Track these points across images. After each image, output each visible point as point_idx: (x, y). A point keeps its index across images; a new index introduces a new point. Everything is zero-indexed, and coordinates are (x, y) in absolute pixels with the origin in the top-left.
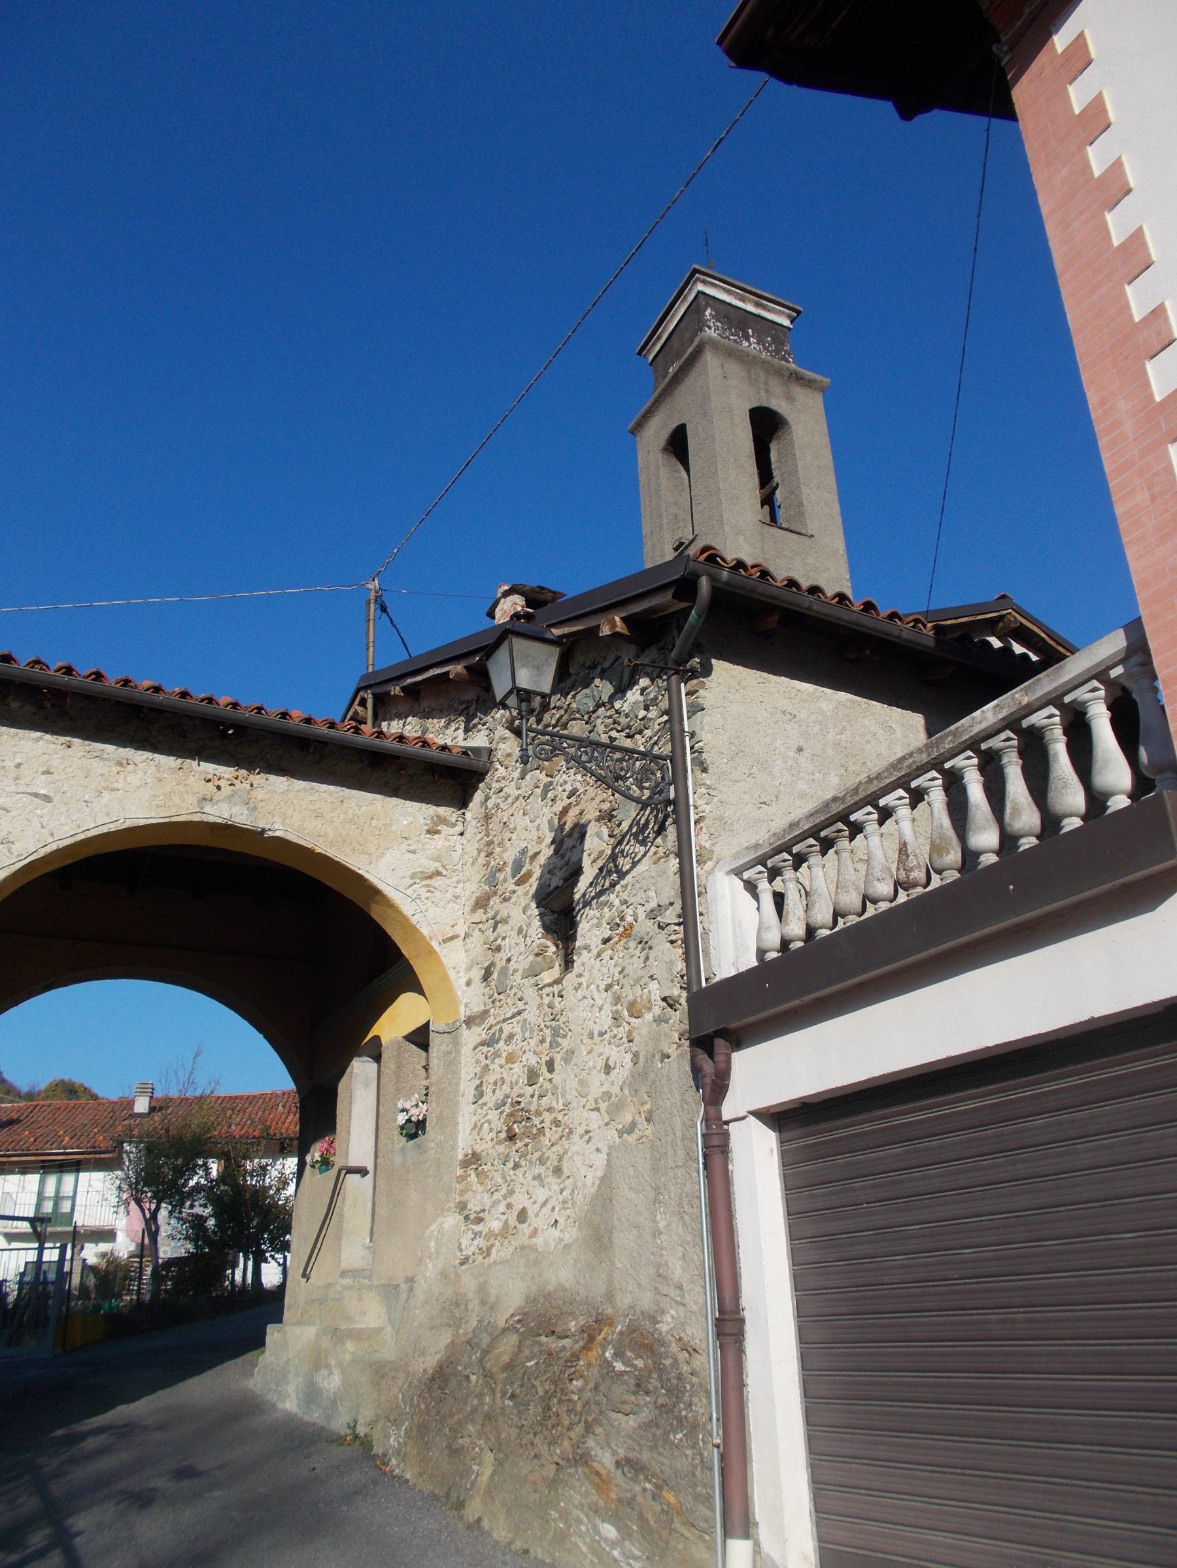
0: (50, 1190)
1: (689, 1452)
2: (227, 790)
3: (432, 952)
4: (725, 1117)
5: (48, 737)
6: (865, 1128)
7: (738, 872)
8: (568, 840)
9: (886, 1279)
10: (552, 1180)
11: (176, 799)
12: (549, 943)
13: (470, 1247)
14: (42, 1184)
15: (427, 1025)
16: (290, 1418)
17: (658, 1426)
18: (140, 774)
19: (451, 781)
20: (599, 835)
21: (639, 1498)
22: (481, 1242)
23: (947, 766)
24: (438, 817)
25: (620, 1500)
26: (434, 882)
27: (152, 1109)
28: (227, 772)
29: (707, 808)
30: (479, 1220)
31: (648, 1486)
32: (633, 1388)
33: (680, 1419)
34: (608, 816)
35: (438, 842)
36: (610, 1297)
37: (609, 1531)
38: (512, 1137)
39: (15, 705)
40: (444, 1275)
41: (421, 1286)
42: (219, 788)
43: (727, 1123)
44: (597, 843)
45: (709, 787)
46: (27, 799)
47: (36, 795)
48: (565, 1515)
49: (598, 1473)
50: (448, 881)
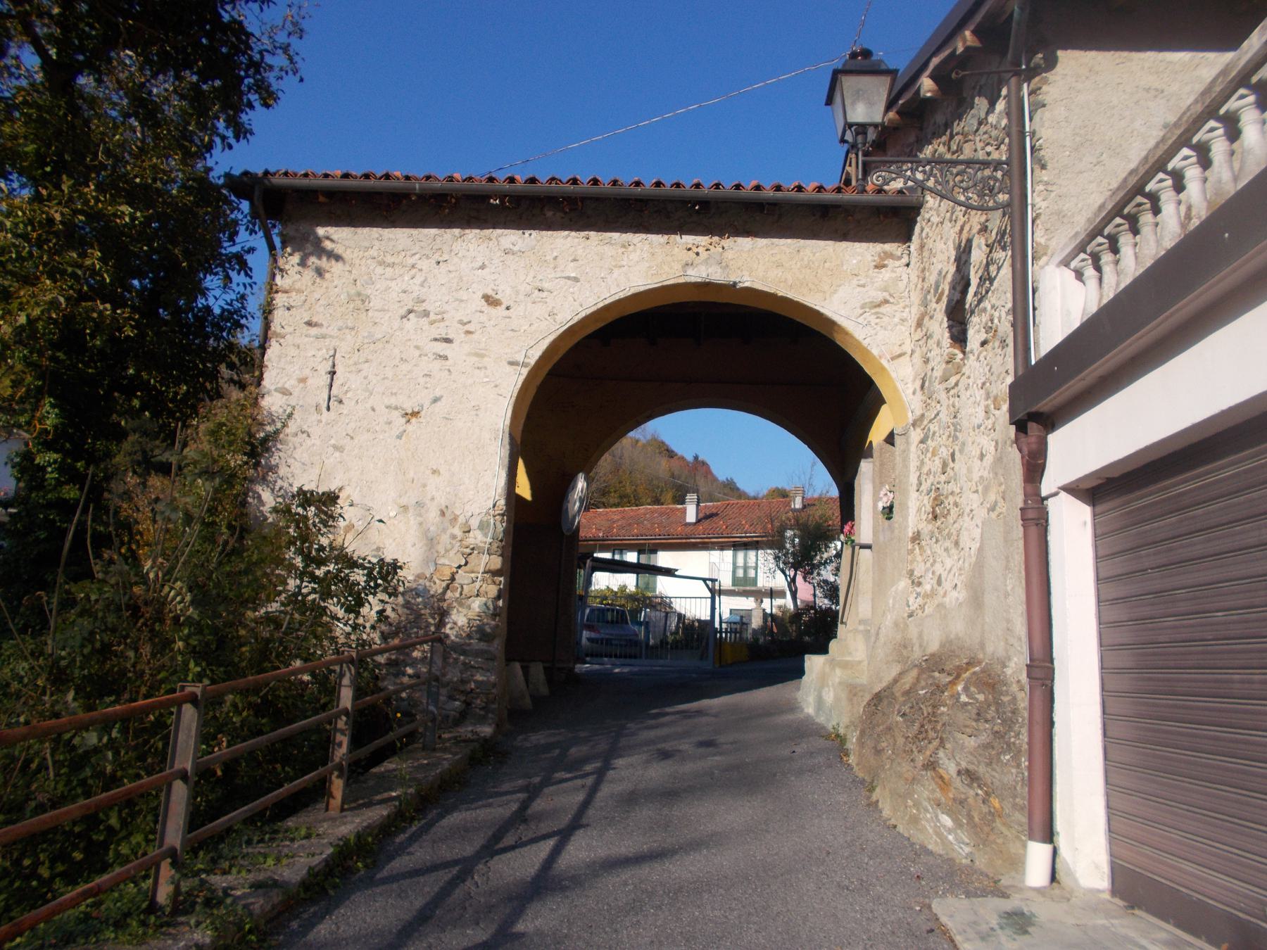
0: (740, 562)
1: (1014, 771)
2: (704, 255)
3: (883, 369)
4: (1044, 494)
5: (573, 233)
6: (1150, 500)
7: (1065, 263)
8: (963, 255)
9: (1161, 638)
10: (953, 551)
11: (666, 268)
12: (957, 351)
13: (914, 604)
14: (735, 557)
15: (1026, 433)
16: (808, 716)
17: (993, 748)
18: (638, 252)
19: (894, 221)
20: (979, 247)
21: (970, 800)
22: (920, 600)
23: (1222, 111)
24: (885, 253)
25: (954, 800)
26: (883, 309)
27: (804, 507)
28: (703, 240)
29: (1044, 205)
30: (919, 584)
31: (980, 792)
32: (974, 716)
33: (1008, 744)
34: (984, 229)
35: (886, 274)
36: (982, 646)
37: (947, 820)
38: (935, 517)
39: (549, 214)
40: (896, 624)
41: (883, 630)
42: (697, 254)
43: (1046, 498)
44: (978, 255)
45: (1047, 183)
46: (563, 282)
47: (569, 278)
48: (917, 804)
49: (941, 777)
50: (895, 308)
